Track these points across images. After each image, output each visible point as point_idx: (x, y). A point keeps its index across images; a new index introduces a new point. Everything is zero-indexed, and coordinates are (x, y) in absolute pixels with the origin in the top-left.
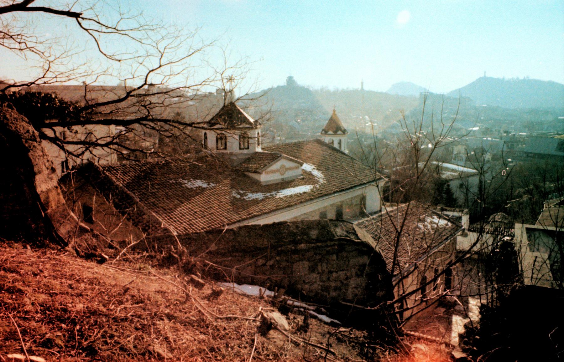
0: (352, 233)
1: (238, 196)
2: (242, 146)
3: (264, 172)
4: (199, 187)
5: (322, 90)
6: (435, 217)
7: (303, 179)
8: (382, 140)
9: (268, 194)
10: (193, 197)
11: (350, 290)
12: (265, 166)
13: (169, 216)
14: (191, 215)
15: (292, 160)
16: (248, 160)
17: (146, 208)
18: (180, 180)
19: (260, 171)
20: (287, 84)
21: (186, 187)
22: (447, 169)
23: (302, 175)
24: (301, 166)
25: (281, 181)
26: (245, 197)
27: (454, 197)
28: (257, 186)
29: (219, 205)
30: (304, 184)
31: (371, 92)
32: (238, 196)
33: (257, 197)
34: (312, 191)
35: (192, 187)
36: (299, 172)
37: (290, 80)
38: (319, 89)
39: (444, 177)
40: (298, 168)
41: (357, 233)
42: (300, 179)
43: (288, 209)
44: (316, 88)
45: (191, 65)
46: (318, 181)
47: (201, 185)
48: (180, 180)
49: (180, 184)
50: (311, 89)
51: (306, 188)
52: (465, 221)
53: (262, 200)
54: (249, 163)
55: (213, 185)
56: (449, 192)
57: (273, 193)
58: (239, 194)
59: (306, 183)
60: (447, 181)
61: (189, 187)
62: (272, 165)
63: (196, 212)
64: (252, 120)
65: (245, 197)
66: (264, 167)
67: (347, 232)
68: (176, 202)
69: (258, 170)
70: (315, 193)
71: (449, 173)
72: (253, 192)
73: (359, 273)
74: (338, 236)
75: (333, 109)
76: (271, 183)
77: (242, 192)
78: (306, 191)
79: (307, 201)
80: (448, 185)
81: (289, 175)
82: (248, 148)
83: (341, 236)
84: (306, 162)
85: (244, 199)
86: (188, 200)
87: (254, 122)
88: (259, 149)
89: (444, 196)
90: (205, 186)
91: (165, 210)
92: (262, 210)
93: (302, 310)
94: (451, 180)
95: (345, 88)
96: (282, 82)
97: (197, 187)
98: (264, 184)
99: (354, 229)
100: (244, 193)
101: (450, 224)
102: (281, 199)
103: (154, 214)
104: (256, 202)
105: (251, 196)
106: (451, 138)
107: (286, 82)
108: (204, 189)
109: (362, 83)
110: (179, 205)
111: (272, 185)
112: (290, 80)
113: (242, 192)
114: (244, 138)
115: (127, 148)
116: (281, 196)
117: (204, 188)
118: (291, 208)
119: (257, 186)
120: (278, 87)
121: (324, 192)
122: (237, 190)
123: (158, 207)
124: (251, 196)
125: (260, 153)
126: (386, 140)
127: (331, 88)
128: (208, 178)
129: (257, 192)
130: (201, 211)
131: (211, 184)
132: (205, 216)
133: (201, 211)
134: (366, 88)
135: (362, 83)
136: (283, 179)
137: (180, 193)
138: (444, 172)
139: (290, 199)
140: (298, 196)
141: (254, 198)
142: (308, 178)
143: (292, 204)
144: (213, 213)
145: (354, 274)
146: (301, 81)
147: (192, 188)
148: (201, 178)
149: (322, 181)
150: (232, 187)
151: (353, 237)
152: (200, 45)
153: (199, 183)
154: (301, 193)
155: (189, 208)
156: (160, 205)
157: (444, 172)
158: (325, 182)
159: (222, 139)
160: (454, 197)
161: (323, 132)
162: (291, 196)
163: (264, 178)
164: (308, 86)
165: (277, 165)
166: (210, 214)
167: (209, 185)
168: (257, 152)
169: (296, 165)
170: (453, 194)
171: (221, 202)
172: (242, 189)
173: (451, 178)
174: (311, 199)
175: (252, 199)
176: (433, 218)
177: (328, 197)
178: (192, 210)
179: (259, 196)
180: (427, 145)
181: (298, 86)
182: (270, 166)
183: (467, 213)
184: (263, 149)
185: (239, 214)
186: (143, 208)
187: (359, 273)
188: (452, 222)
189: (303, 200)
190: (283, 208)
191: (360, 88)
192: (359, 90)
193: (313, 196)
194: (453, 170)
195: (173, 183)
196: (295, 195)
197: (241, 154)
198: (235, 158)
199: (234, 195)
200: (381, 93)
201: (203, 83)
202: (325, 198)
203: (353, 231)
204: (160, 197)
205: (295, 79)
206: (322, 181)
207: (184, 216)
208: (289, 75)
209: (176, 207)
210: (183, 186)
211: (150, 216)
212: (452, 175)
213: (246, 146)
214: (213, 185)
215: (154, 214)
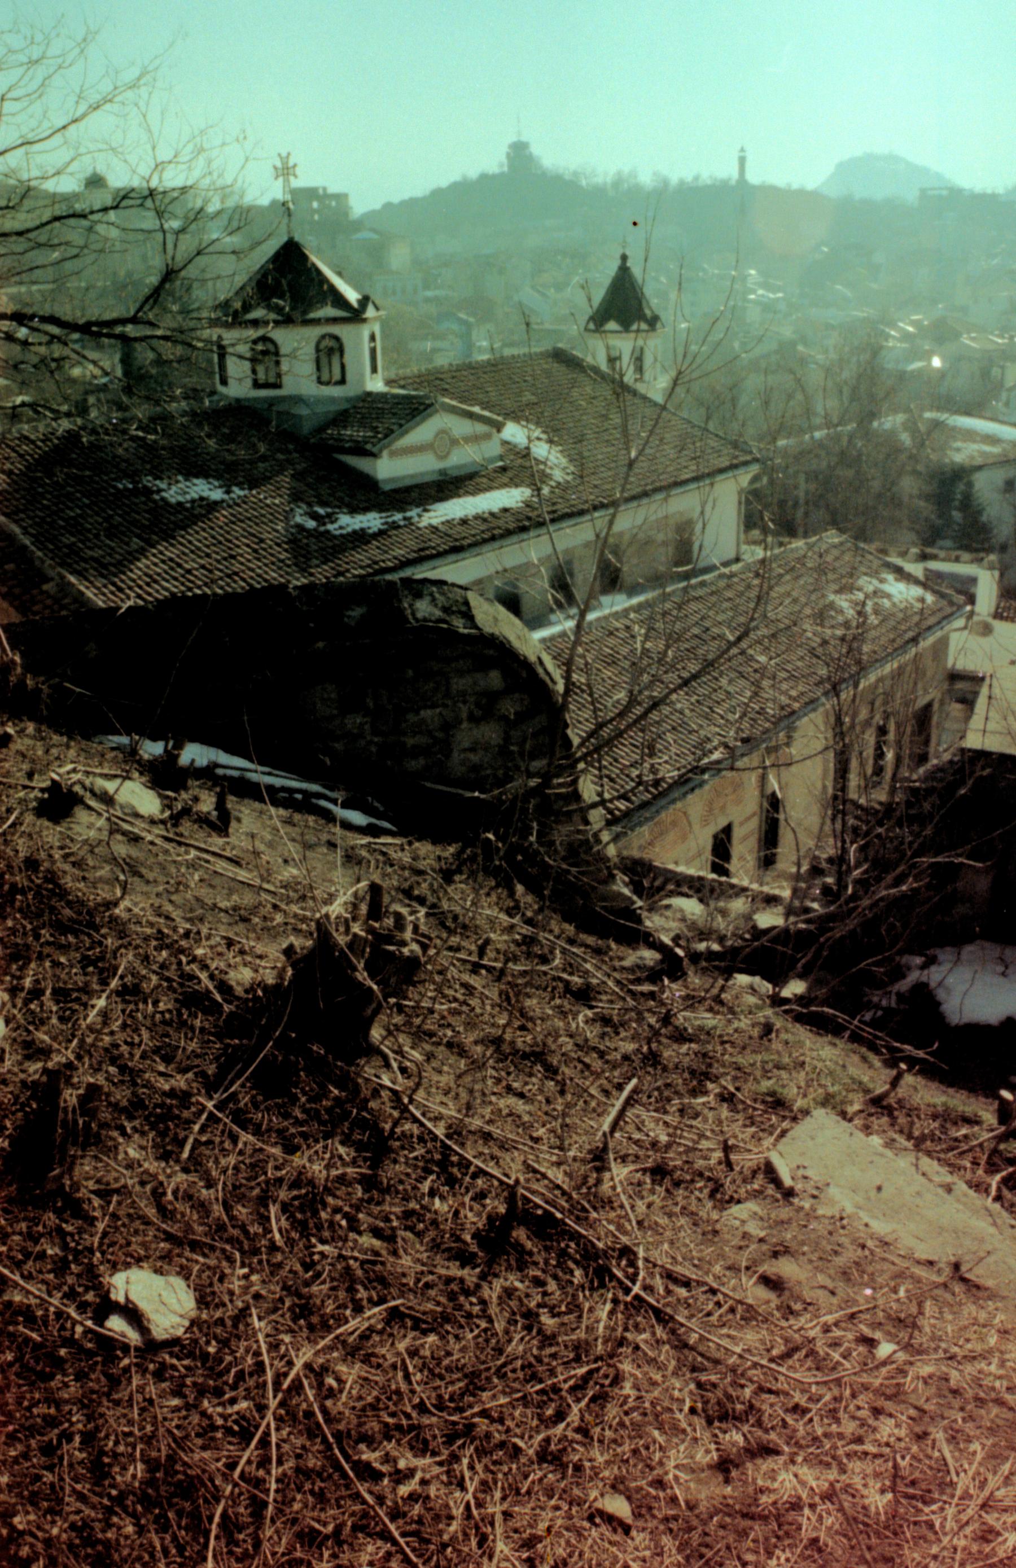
0: (460, 612)
1: (311, 524)
2: (325, 377)
3: (385, 453)
4: (202, 499)
5: (617, 183)
6: (890, 577)
7: (504, 469)
8: (793, 344)
9: (398, 517)
10: (184, 529)
11: (456, 757)
12: (389, 433)
13: (114, 584)
14: (176, 579)
15: (471, 415)
16: (342, 418)
17: (49, 562)
18: (148, 481)
19: (375, 450)
20: (511, 165)
21: (163, 499)
22: (970, 435)
23: (501, 458)
24: (499, 431)
25: (436, 477)
26: (330, 527)
27: (984, 518)
28: (367, 493)
29: (255, 551)
30: (505, 485)
31: (769, 191)
32: (311, 524)
33: (364, 525)
34: (528, 505)
35: (181, 499)
36: (492, 449)
37: (519, 152)
38: (609, 180)
39: (958, 458)
40: (488, 436)
41: (475, 612)
42: (495, 471)
43: (452, 557)
44: (599, 180)
45: (82, 150)
46: (549, 477)
47: (205, 494)
48: (148, 481)
49: (148, 492)
50: (584, 183)
51: (509, 498)
52: (987, 588)
53: (381, 533)
54: (345, 427)
55: (242, 493)
56: (967, 503)
57: (413, 513)
58: (314, 516)
59: (513, 483)
60: (960, 474)
61: (173, 501)
62: (407, 432)
63: (189, 571)
64: (352, 296)
65: (330, 527)
66: (386, 436)
67: (446, 610)
68: (136, 542)
69: (368, 447)
70: (534, 509)
71: (975, 446)
72: (353, 510)
73: (478, 713)
74: (417, 620)
75: (620, 251)
76: (408, 482)
77: (321, 511)
78: (508, 505)
79: (508, 533)
80: (970, 485)
81: (462, 457)
82: (342, 381)
83: (425, 620)
84: (517, 419)
85: (328, 532)
86: (168, 536)
87: (359, 301)
88: (376, 385)
89: (957, 515)
90: (217, 495)
91: (105, 566)
92: (376, 563)
93: (299, 796)
94: (980, 468)
95: (689, 178)
96: (489, 159)
97: (193, 501)
98: (387, 487)
99: (466, 603)
100: (329, 515)
101: (930, 598)
102: (434, 529)
103: (72, 579)
104: (360, 538)
105: (348, 522)
106: (1002, 337)
107: (505, 161)
108: (213, 506)
109: (742, 161)
110: (142, 552)
111: (408, 489)
112: (519, 152)
113: (321, 511)
114: (330, 352)
115: (459, 319)
116: (435, 522)
117: (216, 503)
118: (461, 555)
119: (367, 493)
120: (484, 177)
121: (562, 508)
122: (310, 505)
123: (85, 561)
124: (348, 522)
125: (382, 397)
126: (806, 344)
127: (646, 178)
128: (227, 473)
129: (365, 510)
130: (203, 567)
131: (235, 489)
132: (213, 581)
133: (203, 567)
134: (754, 177)
135: (742, 161)
136: (442, 472)
137: (145, 519)
138: (959, 444)
139: (459, 528)
140: (485, 520)
141: (357, 527)
142: (516, 468)
143: (465, 543)
144: (236, 574)
145: (464, 715)
146: (553, 155)
147: (180, 504)
148: (204, 474)
149: (558, 475)
150: (296, 497)
151: (459, 624)
152: (106, 87)
153: (202, 489)
154: (495, 510)
155: (171, 560)
156: (90, 553)
157: (959, 444)
158: (569, 478)
159: (266, 353)
160: (984, 518)
161: (592, 326)
162: (464, 522)
163: (388, 468)
164: (575, 174)
165: (423, 432)
166: (229, 576)
167: (228, 492)
168: (369, 394)
169: (481, 428)
170: (980, 512)
171: (262, 541)
172: (323, 504)
173: (979, 461)
174: (524, 529)
175: (349, 530)
176: (882, 581)
177: (572, 522)
178: (179, 565)
179: (372, 521)
180: (929, 360)
181: (544, 174)
182: (402, 435)
183: (991, 568)
184: (389, 382)
185: (312, 575)
186: (43, 562)
187: (478, 713)
188: (934, 592)
189: (496, 532)
190: (440, 555)
191: (735, 174)
192: (733, 182)
193: (529, 518)
194: (991, 439)
195: (126, 489)
196: (477, 517)
197: (319, 400)
198: (304, 411)
199: (298, 519)
200: (801, 193)
201: (124, 203)
202: (564, 524)
203: (464, 608)
204: (89, 531)
205: (536, 150)
206: (558, 475)
207: (156, 582)
208: (515, 139)
209: (134, 556)
210: (156, 497)
211: (64, 587)
212: (983, 454)
213: (337, 375)
214: (242, 493)
215: (72, 579)
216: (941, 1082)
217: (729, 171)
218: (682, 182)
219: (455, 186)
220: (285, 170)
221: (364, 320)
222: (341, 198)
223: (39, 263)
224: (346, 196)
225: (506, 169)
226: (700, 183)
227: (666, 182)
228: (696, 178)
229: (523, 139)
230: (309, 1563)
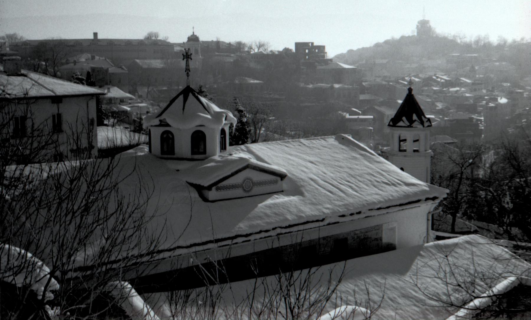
5: (477, 42)
44: (467, 40)
50: (459, 41)
95: (518, 39)
96: (408, 29)
107: (416, 30)
112: (424, 27)
127: (494, 40)
134: (100, 37)
146: (443, 28)
164: (454, 36)
205: (432, 24)
216: (515, 287)
217: (91, 37)
218: (514, 41)
219: (386, 42)
220: (95, 34)
221: (412, 127)
222: (322, 49)
223: (370, 215)
224: (323, 47)
225: (416, 34)
226: (525, 42)
227: (505, 42)
228: (522, 39)
229: (426, 19)
230: (2, 237)
